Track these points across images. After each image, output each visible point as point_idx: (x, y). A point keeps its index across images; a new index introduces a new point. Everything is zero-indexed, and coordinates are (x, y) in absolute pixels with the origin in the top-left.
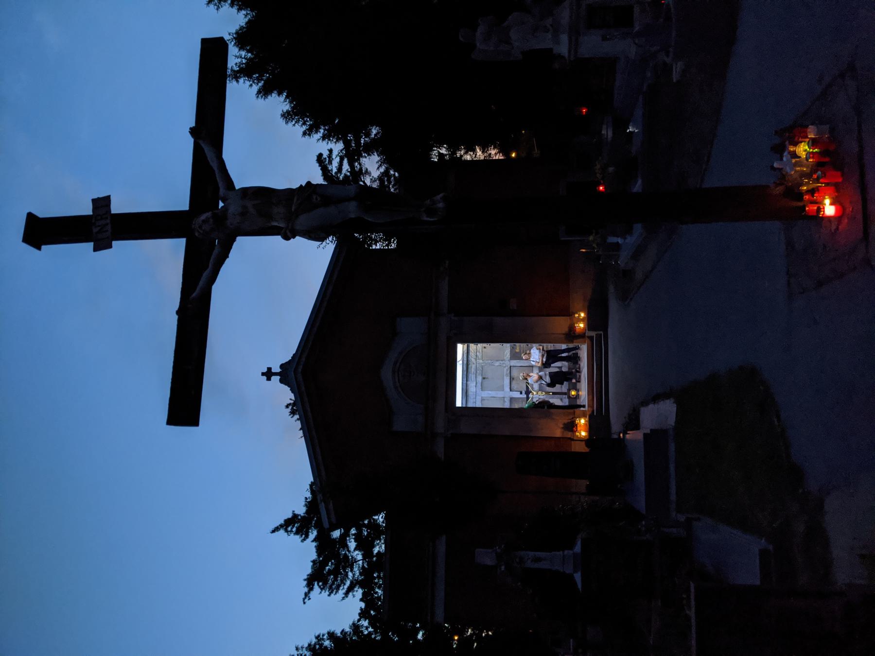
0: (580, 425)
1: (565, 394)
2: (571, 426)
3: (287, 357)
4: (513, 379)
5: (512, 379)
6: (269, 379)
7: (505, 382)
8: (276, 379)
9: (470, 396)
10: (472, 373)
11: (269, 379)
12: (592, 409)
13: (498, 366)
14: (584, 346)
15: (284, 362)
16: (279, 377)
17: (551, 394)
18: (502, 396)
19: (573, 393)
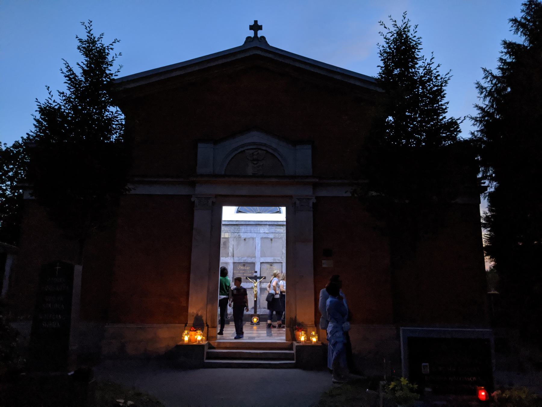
0: (196, 335)
1: (255, 312)
2: (198, 325)
3: (273, 42)
4: (271, 265)
5: (271, 264)
6: (251, 28)
7: (269, 258)
8: (251, 34)
9: (256, 227)
10: (276, 230)
11: (251, 28)
12: (216, 346)
13: (282, 252)
14: (284, 338)
15: (267, 39)
16: (252, 35)
17: (255, 299)
18: (256, 256)
19: (255, 320)
